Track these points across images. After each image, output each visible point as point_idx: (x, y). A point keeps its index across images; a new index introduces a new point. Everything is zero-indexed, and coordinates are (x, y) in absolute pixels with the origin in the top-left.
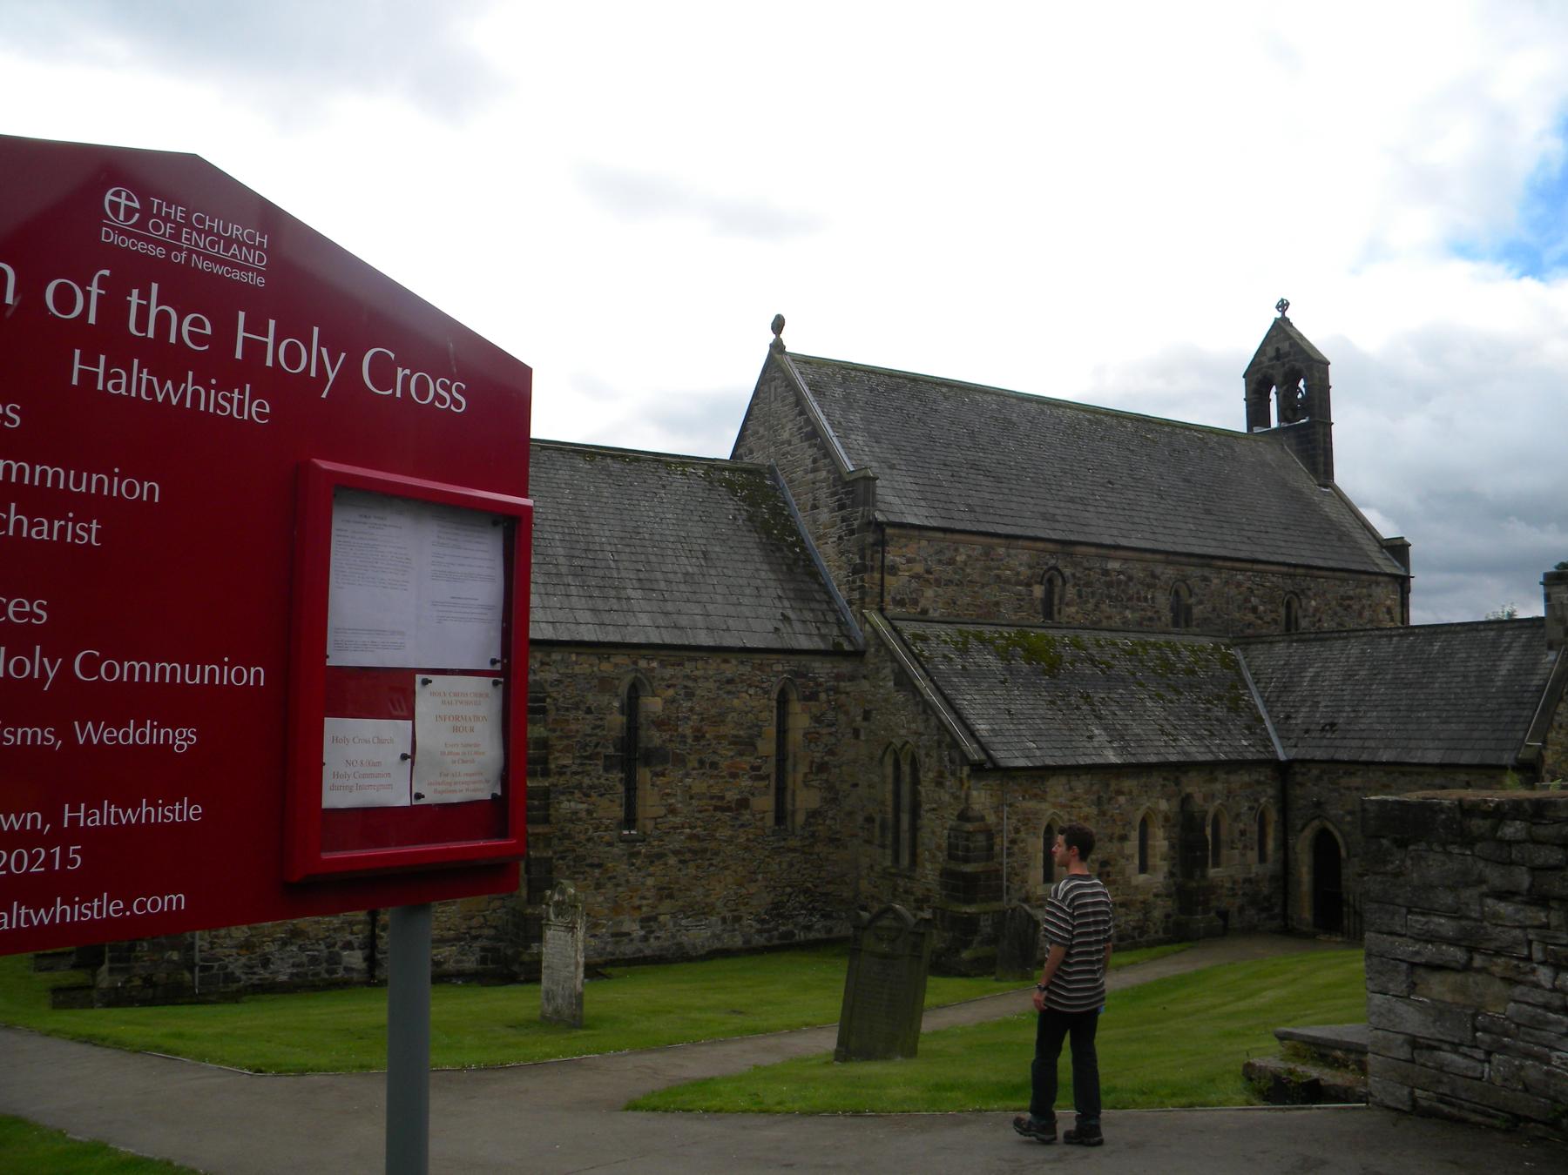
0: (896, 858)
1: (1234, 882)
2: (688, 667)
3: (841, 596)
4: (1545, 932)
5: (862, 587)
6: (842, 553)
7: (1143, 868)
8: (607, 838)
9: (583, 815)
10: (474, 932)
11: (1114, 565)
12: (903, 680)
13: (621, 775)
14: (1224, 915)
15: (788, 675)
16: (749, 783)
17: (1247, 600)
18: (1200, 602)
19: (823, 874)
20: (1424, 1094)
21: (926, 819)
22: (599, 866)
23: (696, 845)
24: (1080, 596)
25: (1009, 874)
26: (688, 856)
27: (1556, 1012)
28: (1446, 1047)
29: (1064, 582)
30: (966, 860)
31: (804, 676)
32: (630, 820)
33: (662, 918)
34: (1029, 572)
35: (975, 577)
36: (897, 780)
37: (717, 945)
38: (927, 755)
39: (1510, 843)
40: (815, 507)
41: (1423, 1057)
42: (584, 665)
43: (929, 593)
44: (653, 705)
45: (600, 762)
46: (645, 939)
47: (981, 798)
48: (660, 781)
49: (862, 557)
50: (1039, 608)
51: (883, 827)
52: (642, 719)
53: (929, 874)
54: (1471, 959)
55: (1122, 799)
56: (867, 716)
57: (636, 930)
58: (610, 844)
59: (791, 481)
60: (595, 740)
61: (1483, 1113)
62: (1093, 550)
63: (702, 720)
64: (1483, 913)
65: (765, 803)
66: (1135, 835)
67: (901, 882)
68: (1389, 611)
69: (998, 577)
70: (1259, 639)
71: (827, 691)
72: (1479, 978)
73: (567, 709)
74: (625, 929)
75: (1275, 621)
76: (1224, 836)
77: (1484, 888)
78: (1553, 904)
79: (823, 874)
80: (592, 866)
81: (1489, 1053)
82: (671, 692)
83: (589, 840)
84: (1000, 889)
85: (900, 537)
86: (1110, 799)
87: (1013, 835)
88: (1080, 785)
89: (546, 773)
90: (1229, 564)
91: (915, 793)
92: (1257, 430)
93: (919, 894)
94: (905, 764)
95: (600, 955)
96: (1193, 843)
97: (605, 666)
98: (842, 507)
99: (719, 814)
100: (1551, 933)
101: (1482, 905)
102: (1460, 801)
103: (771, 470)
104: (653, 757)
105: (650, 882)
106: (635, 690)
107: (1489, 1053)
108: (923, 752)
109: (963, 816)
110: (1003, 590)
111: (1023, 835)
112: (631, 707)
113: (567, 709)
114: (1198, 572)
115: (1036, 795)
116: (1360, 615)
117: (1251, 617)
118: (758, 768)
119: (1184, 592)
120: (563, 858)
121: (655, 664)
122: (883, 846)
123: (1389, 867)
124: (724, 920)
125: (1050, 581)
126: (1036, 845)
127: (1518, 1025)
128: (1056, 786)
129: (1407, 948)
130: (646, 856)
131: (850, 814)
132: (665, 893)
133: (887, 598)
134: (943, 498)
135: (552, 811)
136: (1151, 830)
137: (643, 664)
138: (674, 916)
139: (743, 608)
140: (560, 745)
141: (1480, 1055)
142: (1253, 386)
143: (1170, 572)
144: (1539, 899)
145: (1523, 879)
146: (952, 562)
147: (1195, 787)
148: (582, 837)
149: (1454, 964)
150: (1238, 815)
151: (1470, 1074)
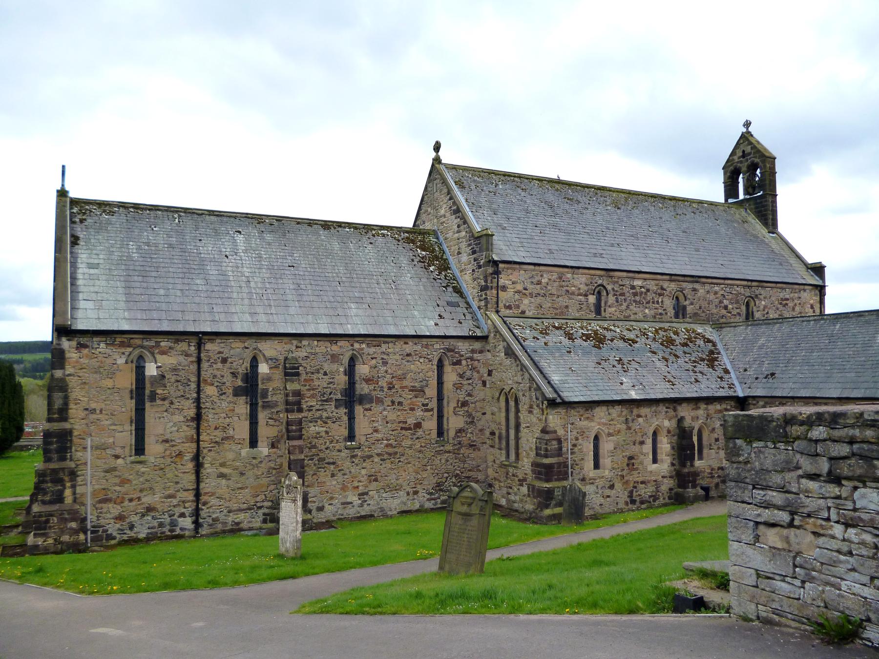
0: (508, 456)
1: (712, 469)
2: (384, 347)
3: (475, 304)
4: (838, 501)
5: (486, 299)
6: (475, 280)
7: (655, 461)
8: (337, 448)
9: (323, 434)
10: (259, 505)
11: (638, 283)
12: (509, 353)
13: (345, 410)
14: (706, 489)
15: (446, 351)
16: (422, 413)
17: (721, 302)
18: (692, 304)
19: (466, 466)
20: (764, 608)
21: (524, 432)
22: (334, 463)
23: (390, 450)
24: (617, 302)
25: (572, 465)
26: (386, 456)
27: (845, 555)
28: (777, 577)
29: (608, 294)
30: (546, 456)
31: (452, 351)
32: (351, 437)
33: (370, 493)
34: (586, 288)
35: (554, 291)
36: (507, 410)
37: (405, 508)
38: (524, 395)
39: (817, 441)
40: (459, 253)
41: (763, 583)
42: (322, 347)
43: (526, 301)
44: (362, 370)
45: (333, 403)
46: (361, 505)
47: (555, 419)
48: (368, 413)
49: (486, 281)
50: (593, 309)
51: (500, 438)
52: (357, 378)
53: (526, 465)
54: (793, 520)
55: (641, 420)
56: (490, 373)
57: (354, 498)
58: (339, 451)
59: (446, 239)
60: (329, 390)
61: (799, 622)
62: (625, 274)
63: (393, 377)
64: (799, 488)
65: (431, 425)
66: (649, 442)
67: (511, 470)
68: (812, 307)
69: (568, 291)
70: (728, 324)
71: (466, 359)
72: (798, 531)
73: (312, 373)
74: (349, 500)
75: (739, 314)
76: (705, 442)
77: (800, 472)
78: (844, 482)
79: (466, 466)
80: (328, 463)
81: (803, 582)
82: (374, 361)
83: (327, 449)
84: (566, 473)
85: (508, 269)
86: (633, 420)
87: (574, 442)
88: (615, 411)
89: (300, 410)
90: (710, 281)
91: (517, 418)
92: (730, 201)
93: (521, 477)
94: (511, 399)
95: (334, 515)
96: (686, 447)
97: (334, 347)
98: (474, 252)
99: (404, 432)
100: (842, 502)
101: (798, 483)
102: (785, 415)
103: (435, 233)
104: (362, 400)
105: (364, 472)
106: (352, 361)
107: (803, 582)
108: (521, 394)
109: (544, 431)
110: (570, 299)
111: (580, 441)
112: (351, 371)
113: (312, 373)
114: (690, 286)
115: (588, 418)
116: (793, 309)
117: (724, 312)
118: (427, 405)
119: (681, 298)
120: (312, 460)
121: (364, 346)
122: (500, 449)
123: (741, 459)
124: (408, 494)
125: (599, 293)
126: (588, 447)
127: (822, 564)
128: (600, 412)
129: (752, 512)
130: (361, 457)
131: (481, 430)
132: (373, 478)
133: (501, 305)
134: (534, 245)
135: (304, 432)
136: (659, 438)
137: (357, 346)
138: (378, 491)
139: (419, 311)
140: (308, 394)
141: (798, 583)
142: (728, 174)
143: (671, 287)
144: (835, 479)
145: (824, 466)
146: (539, 283)
147: (685, 411)
148: (323, 447)
149: (782, 523)
150: (714, 429)
151: (792, 596)
